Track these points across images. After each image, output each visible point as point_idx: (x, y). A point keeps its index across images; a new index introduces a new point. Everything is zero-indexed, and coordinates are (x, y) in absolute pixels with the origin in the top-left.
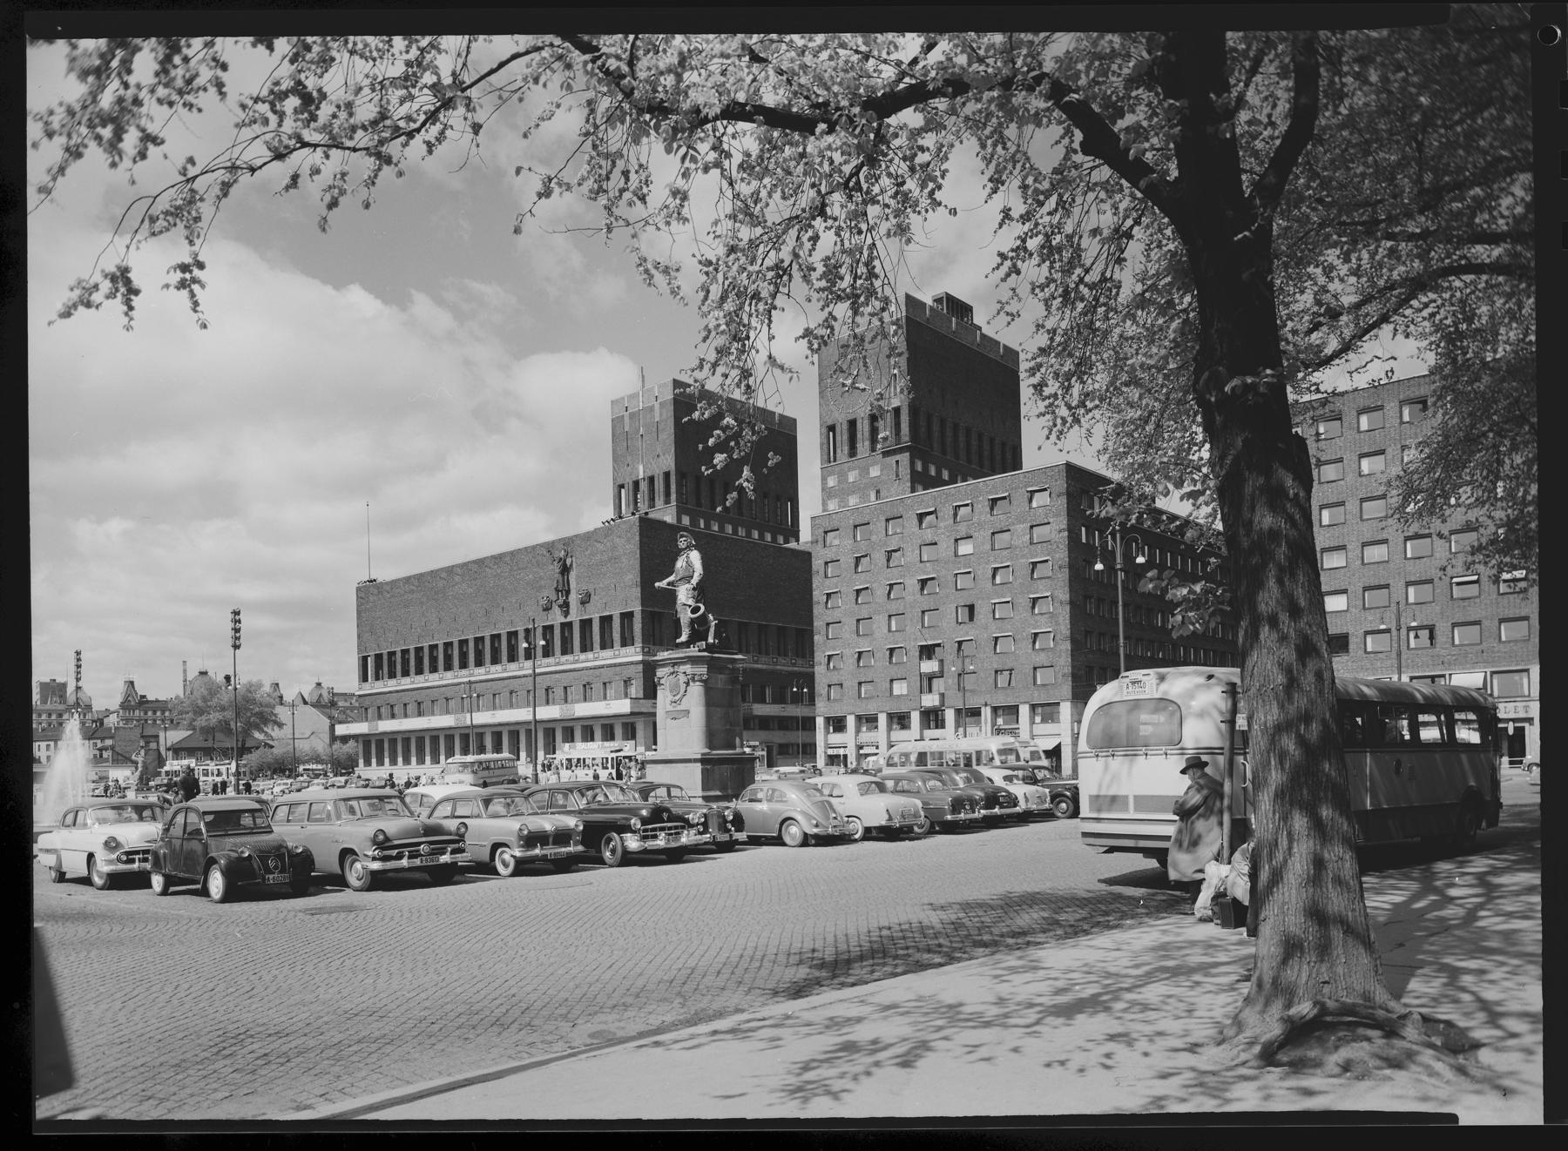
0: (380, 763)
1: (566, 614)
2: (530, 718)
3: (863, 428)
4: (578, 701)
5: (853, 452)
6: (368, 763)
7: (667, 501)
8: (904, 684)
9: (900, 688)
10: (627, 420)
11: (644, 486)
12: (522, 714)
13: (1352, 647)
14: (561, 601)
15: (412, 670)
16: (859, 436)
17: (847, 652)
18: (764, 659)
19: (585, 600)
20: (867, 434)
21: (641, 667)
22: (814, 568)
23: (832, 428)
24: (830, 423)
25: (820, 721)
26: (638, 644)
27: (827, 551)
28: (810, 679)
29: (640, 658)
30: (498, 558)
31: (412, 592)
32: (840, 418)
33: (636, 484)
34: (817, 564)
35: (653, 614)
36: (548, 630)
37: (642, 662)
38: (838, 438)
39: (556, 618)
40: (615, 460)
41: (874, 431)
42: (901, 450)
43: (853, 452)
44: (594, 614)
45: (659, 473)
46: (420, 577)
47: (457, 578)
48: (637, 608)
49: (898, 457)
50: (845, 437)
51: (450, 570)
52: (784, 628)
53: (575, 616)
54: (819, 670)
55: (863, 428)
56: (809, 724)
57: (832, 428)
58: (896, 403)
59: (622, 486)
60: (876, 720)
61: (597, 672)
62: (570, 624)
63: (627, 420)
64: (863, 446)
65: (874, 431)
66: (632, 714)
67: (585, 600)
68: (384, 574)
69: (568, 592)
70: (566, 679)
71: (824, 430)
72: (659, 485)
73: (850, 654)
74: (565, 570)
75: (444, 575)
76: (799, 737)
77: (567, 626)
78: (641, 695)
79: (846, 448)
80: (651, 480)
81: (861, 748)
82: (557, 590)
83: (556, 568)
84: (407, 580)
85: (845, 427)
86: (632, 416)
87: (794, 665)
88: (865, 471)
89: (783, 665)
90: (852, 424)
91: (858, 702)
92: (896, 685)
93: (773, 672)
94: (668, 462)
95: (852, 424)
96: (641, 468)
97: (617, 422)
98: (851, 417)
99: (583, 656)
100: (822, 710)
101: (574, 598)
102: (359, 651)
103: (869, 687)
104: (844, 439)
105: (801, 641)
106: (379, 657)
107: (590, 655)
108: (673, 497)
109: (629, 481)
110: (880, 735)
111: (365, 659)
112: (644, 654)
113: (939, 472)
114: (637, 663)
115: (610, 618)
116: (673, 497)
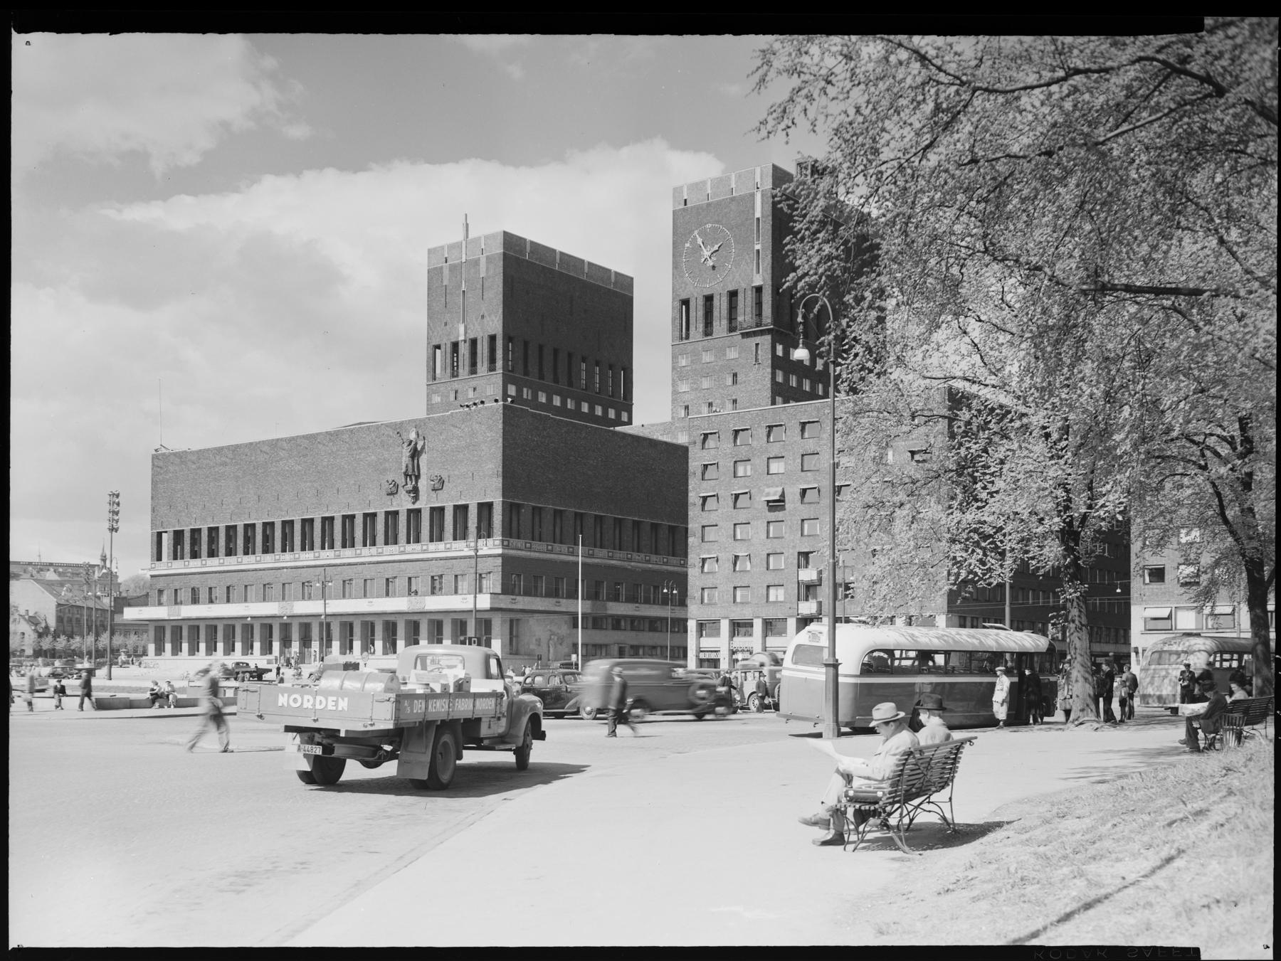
0: (194, 650)
1: (416, 498)
2: (470, 606)
3: (721, 306)
4: (296, 599)
5: (708, 331)
6: (160, 650)
7: (492, 367)
8: (781, 591)
9: (777, 595)
10: (446, 272)
11: (464, 350)
12: (398, 604)
13: (1167, 577)
14: (410, 487)
15: (222, 550)
16: (716, 313)
17: (722, 556)
18: (618, 554)
19: (439, 484)
20: (725, 312)
21: (499, 561)
22: (691, 469)
23: (686, 302)
24: (684, 296)
25: (692, 625)
26: (497, 537)
27: (705, 452)
28: (681, 581)
29: (500, 551)
30: (334, 436)
31: (225, 464)
32: (696, 294)
33: (455, 346)
34: (694, 465)
35: (512, 505)
36: (392, 515)
37: (502, 555)
38: (692, 314)
39: (403, 503)
40: (430, 317)
41: (732, 308)
42: (762, 333)
43: (708, 331)
44: (448, 501)
45: (482, 334)
46: (235, 449)
47: (282, 454)
48: (497, 499)
49: (758, 339)
50: (701, 313)
51: (274, 444)
52: (620, 520)
53: (424, 504)
54: (693, 573)
55: (721, 306)
56: (681, 625)
57: (686, 302)
58: (758, 282)
59: (438, 347)
60: (751, 625)
61: (449, 563)
62: (419, 511)
63: (446, 272)
64: (720, 325)
65: (732, 308)
66: (492, 609)
67: (439, 484)
68: (177, 443)
69: (418, 477)
70: (411, 570)
71: (677, 304)
72: (483, 349)
73: (726, 557)
74: (415, 454)
75: (266, 448)
76: (668, 639)
77: (415, 514)
78: (499, 591)
79: (701, 327)
80: (474, 342)
81: (733, 653)
82: (406, 475)
83: (406, 452)
84: (219, 450)
85: (701, 302)
86: (453, 268)
87: (648, 562)
88: (721, 352)
89: (657, 563)
90: (709, 299)
91: (734, 608)
92: (772, 591)
93: (645, 571)
94: (495, 324)
95: (709, 299)
96: (462, 328)
97: (434, 274)
98: (708, 293)
99: (432, 546)
100: (695, 613)
101: (423, 484)
102: (153, 525)
103: (745, 591)
104: (698, 315)
105: (673, 538)
106: (178, 535)
107: (441, 546)
108: (499, 363)
109: (446, 343)
110: (754, 640)
111: (159, 535)
112: (504, 547)
113: (813, 387)
114: (499, 555)
115: (466, 507)
116: (499, 363)
